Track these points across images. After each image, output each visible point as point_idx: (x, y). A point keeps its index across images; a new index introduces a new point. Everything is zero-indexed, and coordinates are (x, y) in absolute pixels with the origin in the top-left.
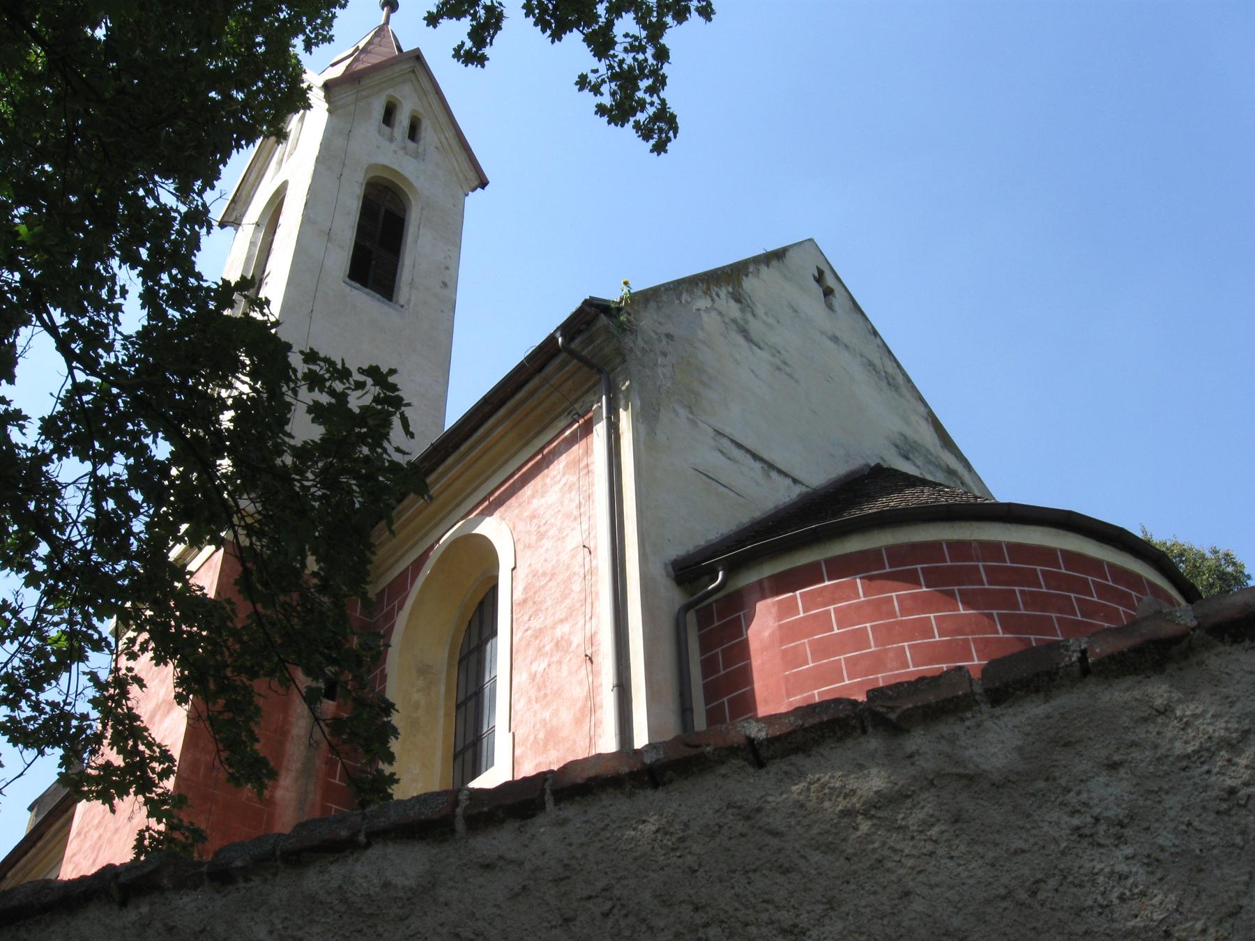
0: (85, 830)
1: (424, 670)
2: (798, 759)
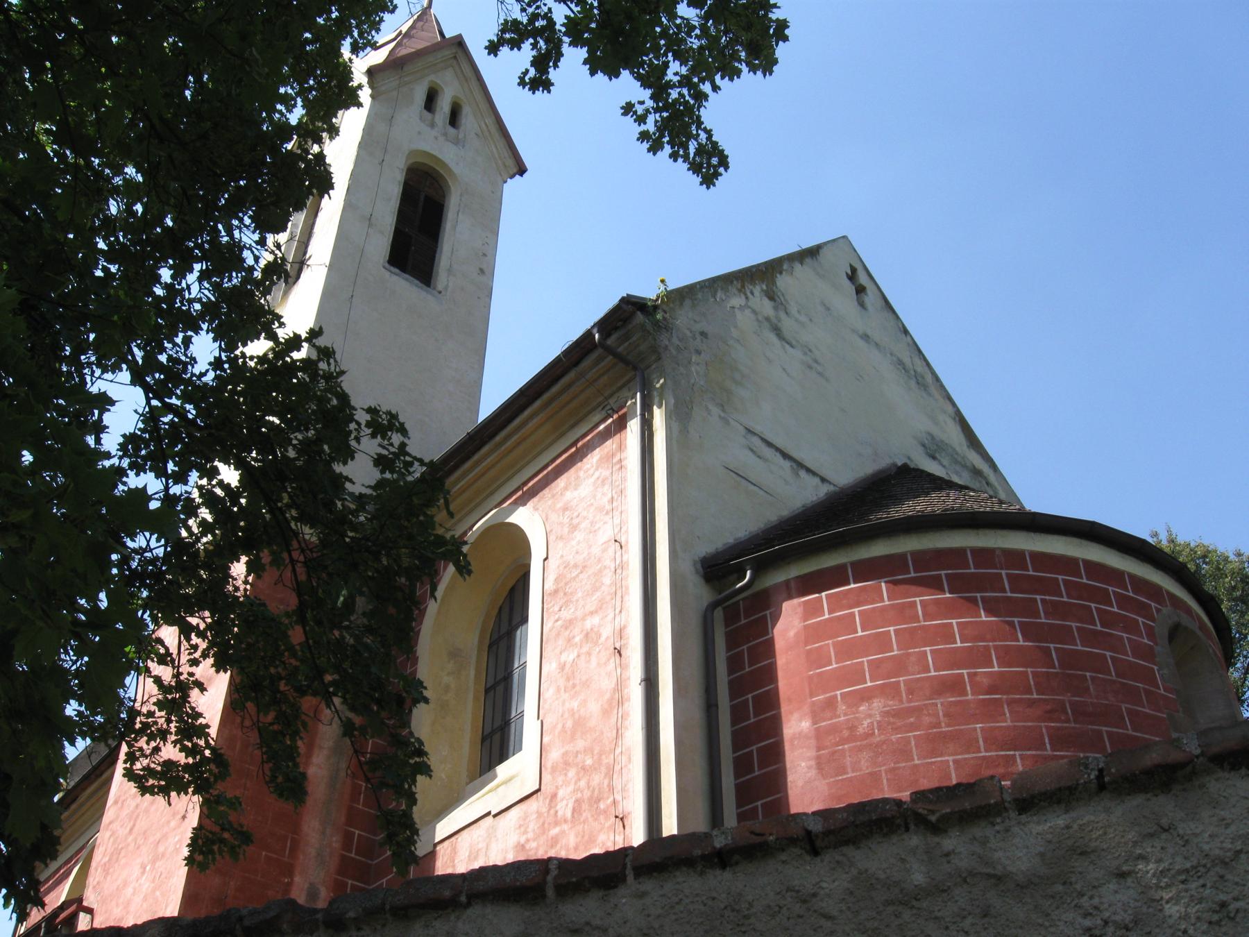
0: (123, 798)
1: (455, 654)
2: (849, 851)
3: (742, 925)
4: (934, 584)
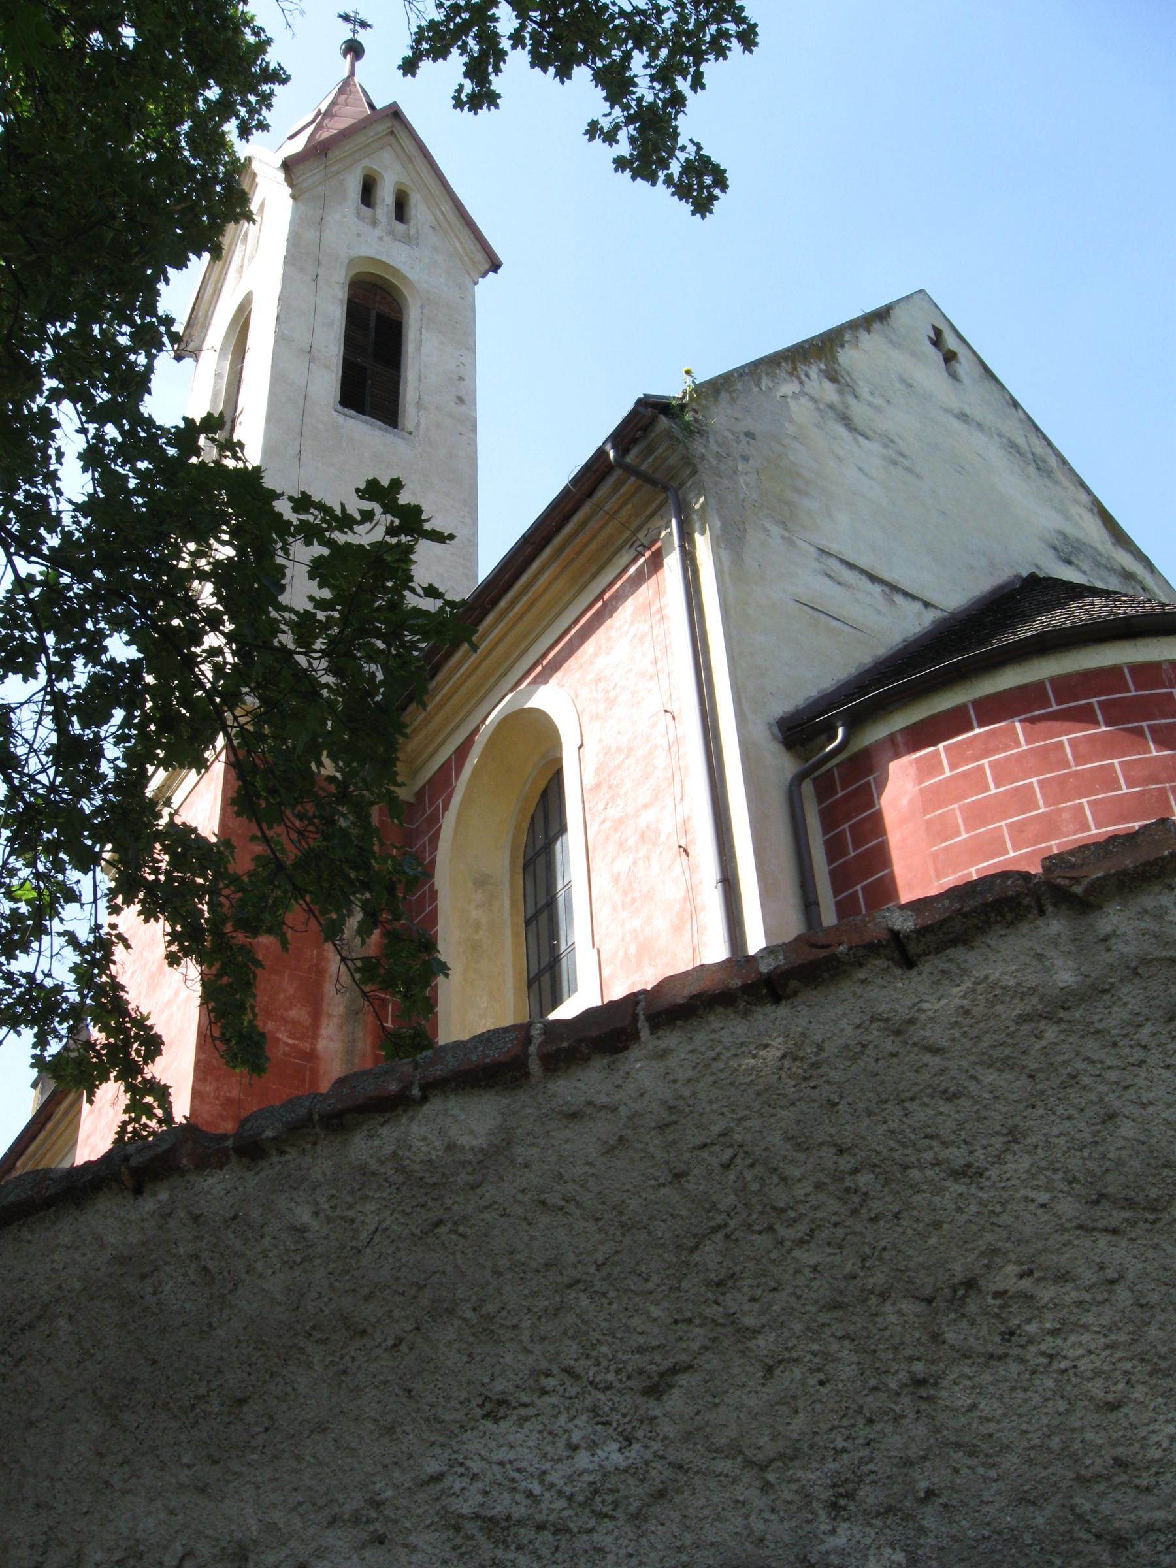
2: (959, 953)
3: (811, 1077)
4: (1085, 716)
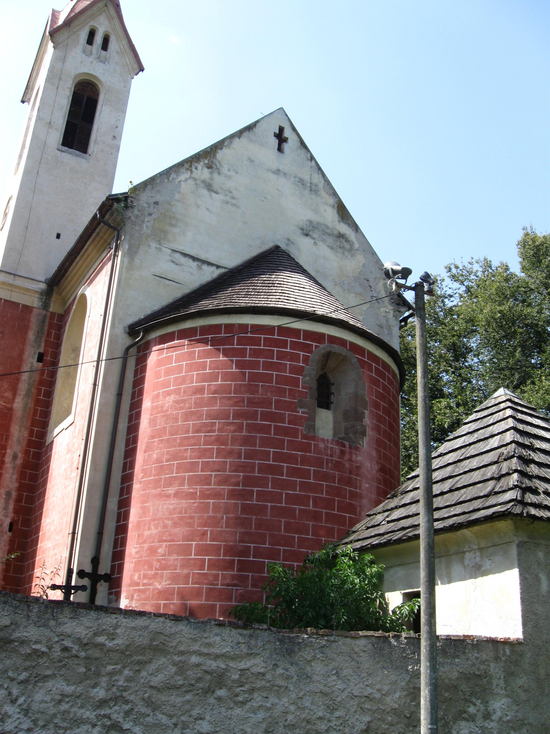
4: (205, 342)
